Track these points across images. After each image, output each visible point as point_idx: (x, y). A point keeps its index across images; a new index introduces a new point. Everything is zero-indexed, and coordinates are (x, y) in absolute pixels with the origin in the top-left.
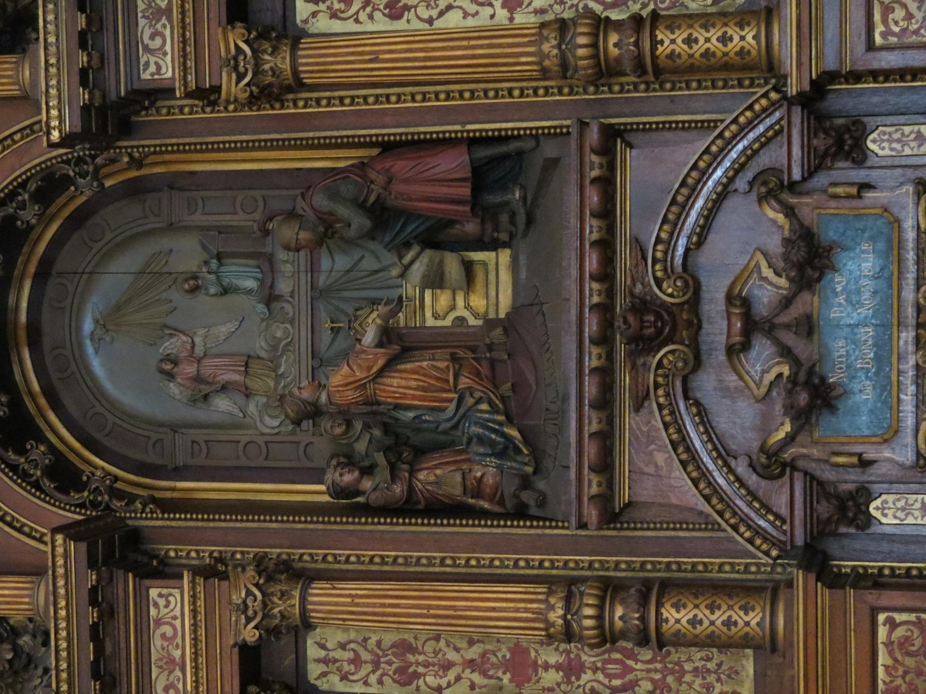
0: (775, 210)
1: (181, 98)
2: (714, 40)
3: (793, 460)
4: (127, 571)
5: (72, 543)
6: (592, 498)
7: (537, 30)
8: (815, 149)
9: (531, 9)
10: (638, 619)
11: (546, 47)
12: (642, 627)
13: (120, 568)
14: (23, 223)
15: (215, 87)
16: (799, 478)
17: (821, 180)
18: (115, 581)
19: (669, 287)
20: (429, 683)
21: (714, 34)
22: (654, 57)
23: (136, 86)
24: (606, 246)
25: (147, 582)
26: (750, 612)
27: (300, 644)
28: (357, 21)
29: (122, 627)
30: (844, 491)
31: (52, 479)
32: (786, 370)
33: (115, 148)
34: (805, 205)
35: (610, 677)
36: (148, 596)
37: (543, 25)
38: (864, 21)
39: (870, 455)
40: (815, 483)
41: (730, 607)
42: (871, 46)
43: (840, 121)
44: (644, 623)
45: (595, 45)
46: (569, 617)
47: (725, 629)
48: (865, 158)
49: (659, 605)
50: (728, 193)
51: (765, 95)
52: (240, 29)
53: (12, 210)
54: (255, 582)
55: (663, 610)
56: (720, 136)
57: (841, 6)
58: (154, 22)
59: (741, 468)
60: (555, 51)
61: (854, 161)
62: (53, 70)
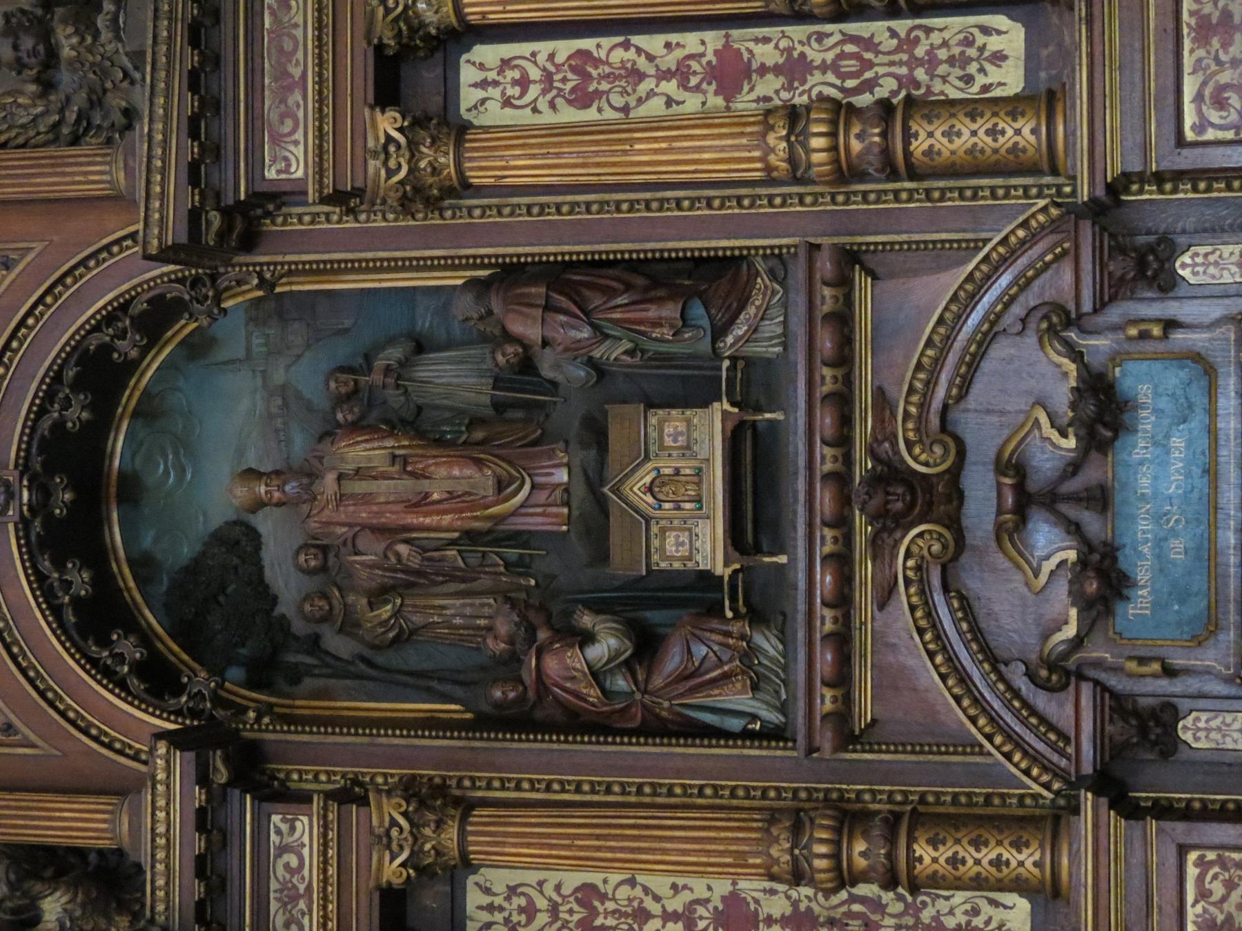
0: (1059, 353)
1: (314, 203)
2: (981, 133)
3: (1079, 667)
4: (245, 791)
5: (178, 753)
6: (825, 717)
7: (766, 825)
8: (1110, 274)
9: (753, 96)
10: (879, 135)
11: (774, 852)
12: (889, 866)
13: (235, 787)
14: (120, 356)
15: (359, 189)
16: (1086, 690)
17: (1114, 314)
18: (229, 892)
19: (923, 452)
20: (617, 105)
21: (983, 125)
22: (907, 154)
23: (260, 187)
24: (843, 401)
25: (266, 806)
26: (1019, 118)
27: (450, 74)
28: (535, 110)
29: (230, 123)
30: (1142, 245)
31: (142, 679)
32: (1072, 555)
33: (233, 266)
34: (1098, 345)
35: (843, 76)
36: (269, 821)
37: (768, 113)
38: (1175, 893)
39: (1178, 662)
40: (1107, 696)
41: (999, 843)
42: (1181, 142)
43: (1141, 240)
44: (891, 862)
45: (834, 148)
46: (797, 852)
47: (993, 870)
48: (1175, 750)
49: (911, 840)
50: (996, 334)
51: (1044, 210)
52: (392, 113)
53: (108, 338)
54: (403, 809)
55: (916, 847)
56: (986, 259)
57: (1146, 844)
58: (289, 907)
59: (1017, 676)
60: (784, 144)
61: (1162, 289)
62: (161, 841)
